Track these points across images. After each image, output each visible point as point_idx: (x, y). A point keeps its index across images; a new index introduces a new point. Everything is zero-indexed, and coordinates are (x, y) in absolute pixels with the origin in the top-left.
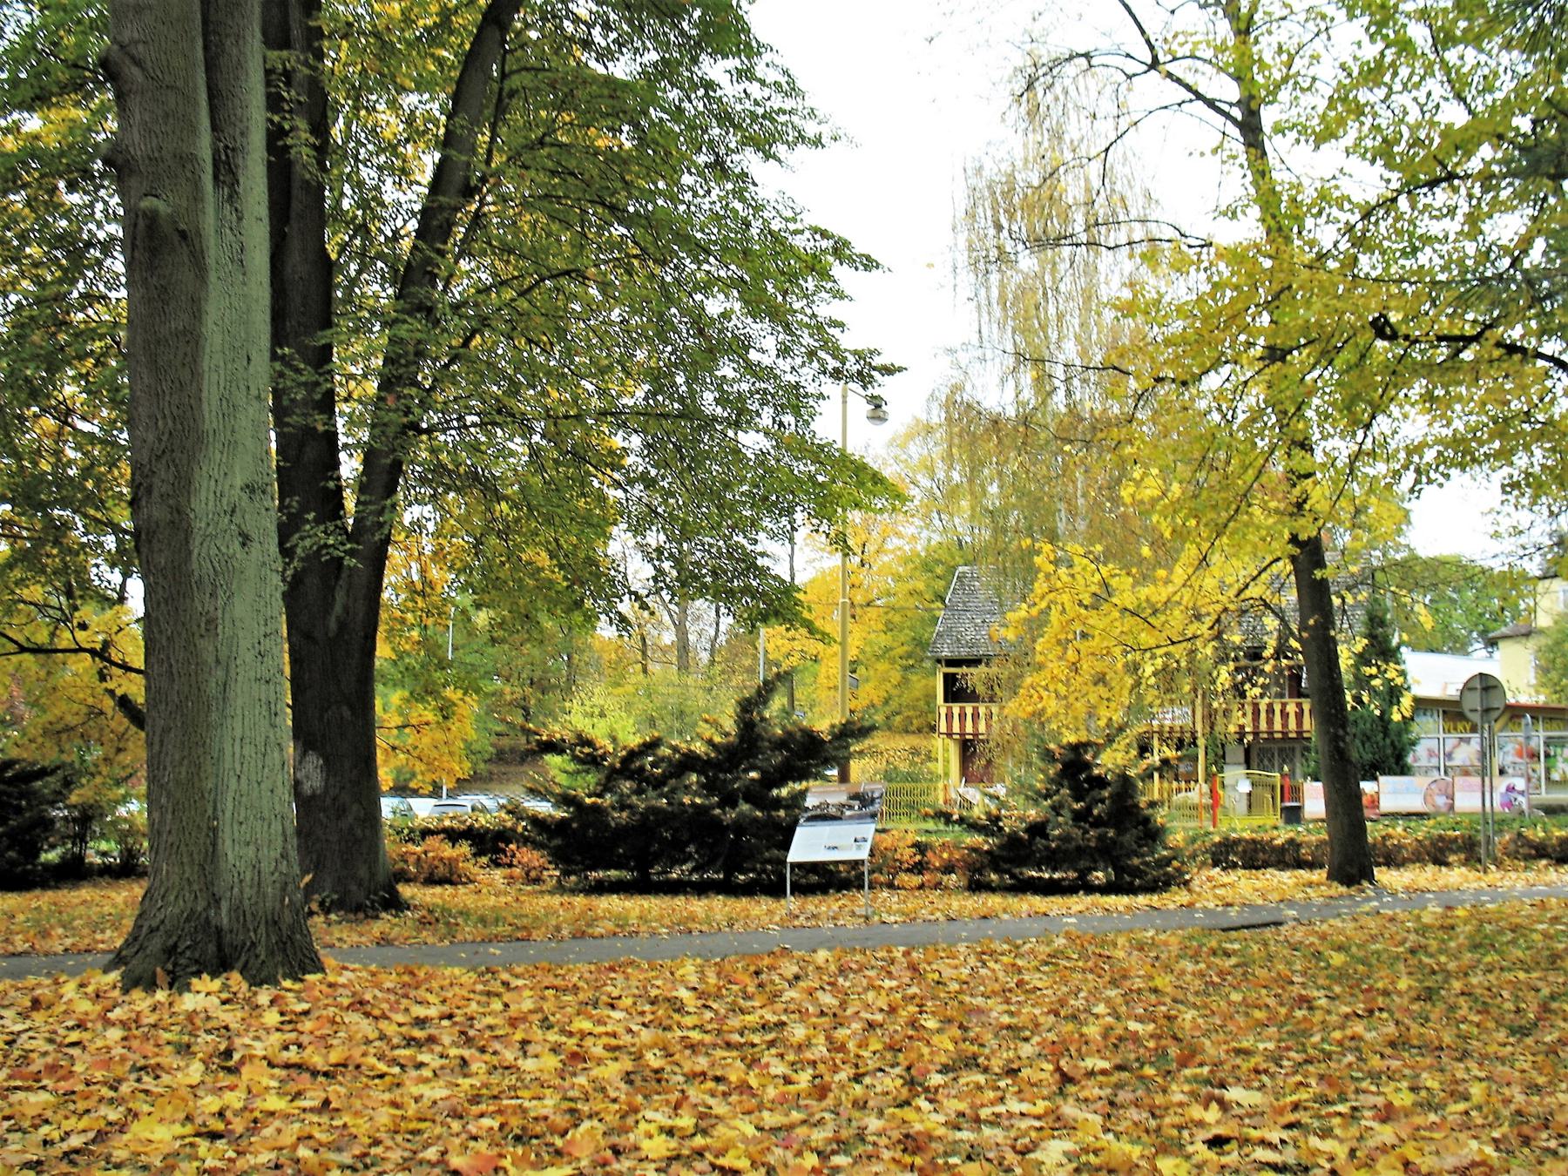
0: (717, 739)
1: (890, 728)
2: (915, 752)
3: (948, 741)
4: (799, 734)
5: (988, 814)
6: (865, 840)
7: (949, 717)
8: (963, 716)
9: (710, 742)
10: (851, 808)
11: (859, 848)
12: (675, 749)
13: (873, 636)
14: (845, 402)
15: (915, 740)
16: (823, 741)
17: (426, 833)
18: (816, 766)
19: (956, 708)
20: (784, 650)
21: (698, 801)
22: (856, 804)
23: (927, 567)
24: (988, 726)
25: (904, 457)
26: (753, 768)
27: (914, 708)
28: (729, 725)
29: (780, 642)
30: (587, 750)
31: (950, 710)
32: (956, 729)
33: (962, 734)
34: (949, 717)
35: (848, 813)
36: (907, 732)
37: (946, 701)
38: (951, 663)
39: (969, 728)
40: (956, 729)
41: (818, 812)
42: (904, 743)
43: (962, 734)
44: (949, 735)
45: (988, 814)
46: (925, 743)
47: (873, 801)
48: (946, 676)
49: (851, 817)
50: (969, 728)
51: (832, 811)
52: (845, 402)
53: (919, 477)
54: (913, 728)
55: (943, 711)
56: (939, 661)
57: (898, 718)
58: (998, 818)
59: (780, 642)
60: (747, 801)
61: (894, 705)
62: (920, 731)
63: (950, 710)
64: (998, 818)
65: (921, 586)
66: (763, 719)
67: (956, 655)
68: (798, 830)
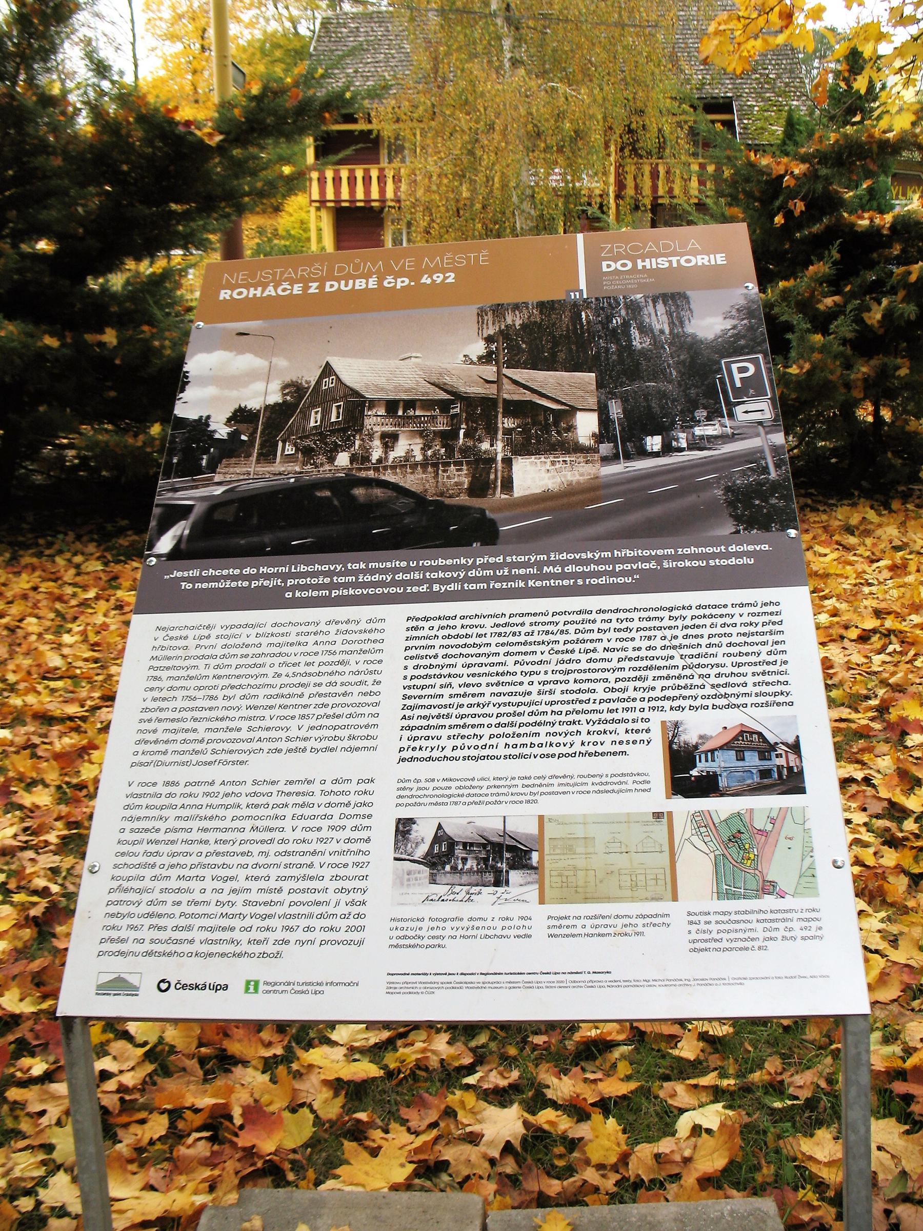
4: (138, 134)
7: (322, 181)
18: (186, 216)
32: (330, 195)
33: (337, 201)
34: (322, 181)
39: (345, 194)
40: (330, 195)
43: (337, 201)
46: (269, 222)
50: (345, 194)
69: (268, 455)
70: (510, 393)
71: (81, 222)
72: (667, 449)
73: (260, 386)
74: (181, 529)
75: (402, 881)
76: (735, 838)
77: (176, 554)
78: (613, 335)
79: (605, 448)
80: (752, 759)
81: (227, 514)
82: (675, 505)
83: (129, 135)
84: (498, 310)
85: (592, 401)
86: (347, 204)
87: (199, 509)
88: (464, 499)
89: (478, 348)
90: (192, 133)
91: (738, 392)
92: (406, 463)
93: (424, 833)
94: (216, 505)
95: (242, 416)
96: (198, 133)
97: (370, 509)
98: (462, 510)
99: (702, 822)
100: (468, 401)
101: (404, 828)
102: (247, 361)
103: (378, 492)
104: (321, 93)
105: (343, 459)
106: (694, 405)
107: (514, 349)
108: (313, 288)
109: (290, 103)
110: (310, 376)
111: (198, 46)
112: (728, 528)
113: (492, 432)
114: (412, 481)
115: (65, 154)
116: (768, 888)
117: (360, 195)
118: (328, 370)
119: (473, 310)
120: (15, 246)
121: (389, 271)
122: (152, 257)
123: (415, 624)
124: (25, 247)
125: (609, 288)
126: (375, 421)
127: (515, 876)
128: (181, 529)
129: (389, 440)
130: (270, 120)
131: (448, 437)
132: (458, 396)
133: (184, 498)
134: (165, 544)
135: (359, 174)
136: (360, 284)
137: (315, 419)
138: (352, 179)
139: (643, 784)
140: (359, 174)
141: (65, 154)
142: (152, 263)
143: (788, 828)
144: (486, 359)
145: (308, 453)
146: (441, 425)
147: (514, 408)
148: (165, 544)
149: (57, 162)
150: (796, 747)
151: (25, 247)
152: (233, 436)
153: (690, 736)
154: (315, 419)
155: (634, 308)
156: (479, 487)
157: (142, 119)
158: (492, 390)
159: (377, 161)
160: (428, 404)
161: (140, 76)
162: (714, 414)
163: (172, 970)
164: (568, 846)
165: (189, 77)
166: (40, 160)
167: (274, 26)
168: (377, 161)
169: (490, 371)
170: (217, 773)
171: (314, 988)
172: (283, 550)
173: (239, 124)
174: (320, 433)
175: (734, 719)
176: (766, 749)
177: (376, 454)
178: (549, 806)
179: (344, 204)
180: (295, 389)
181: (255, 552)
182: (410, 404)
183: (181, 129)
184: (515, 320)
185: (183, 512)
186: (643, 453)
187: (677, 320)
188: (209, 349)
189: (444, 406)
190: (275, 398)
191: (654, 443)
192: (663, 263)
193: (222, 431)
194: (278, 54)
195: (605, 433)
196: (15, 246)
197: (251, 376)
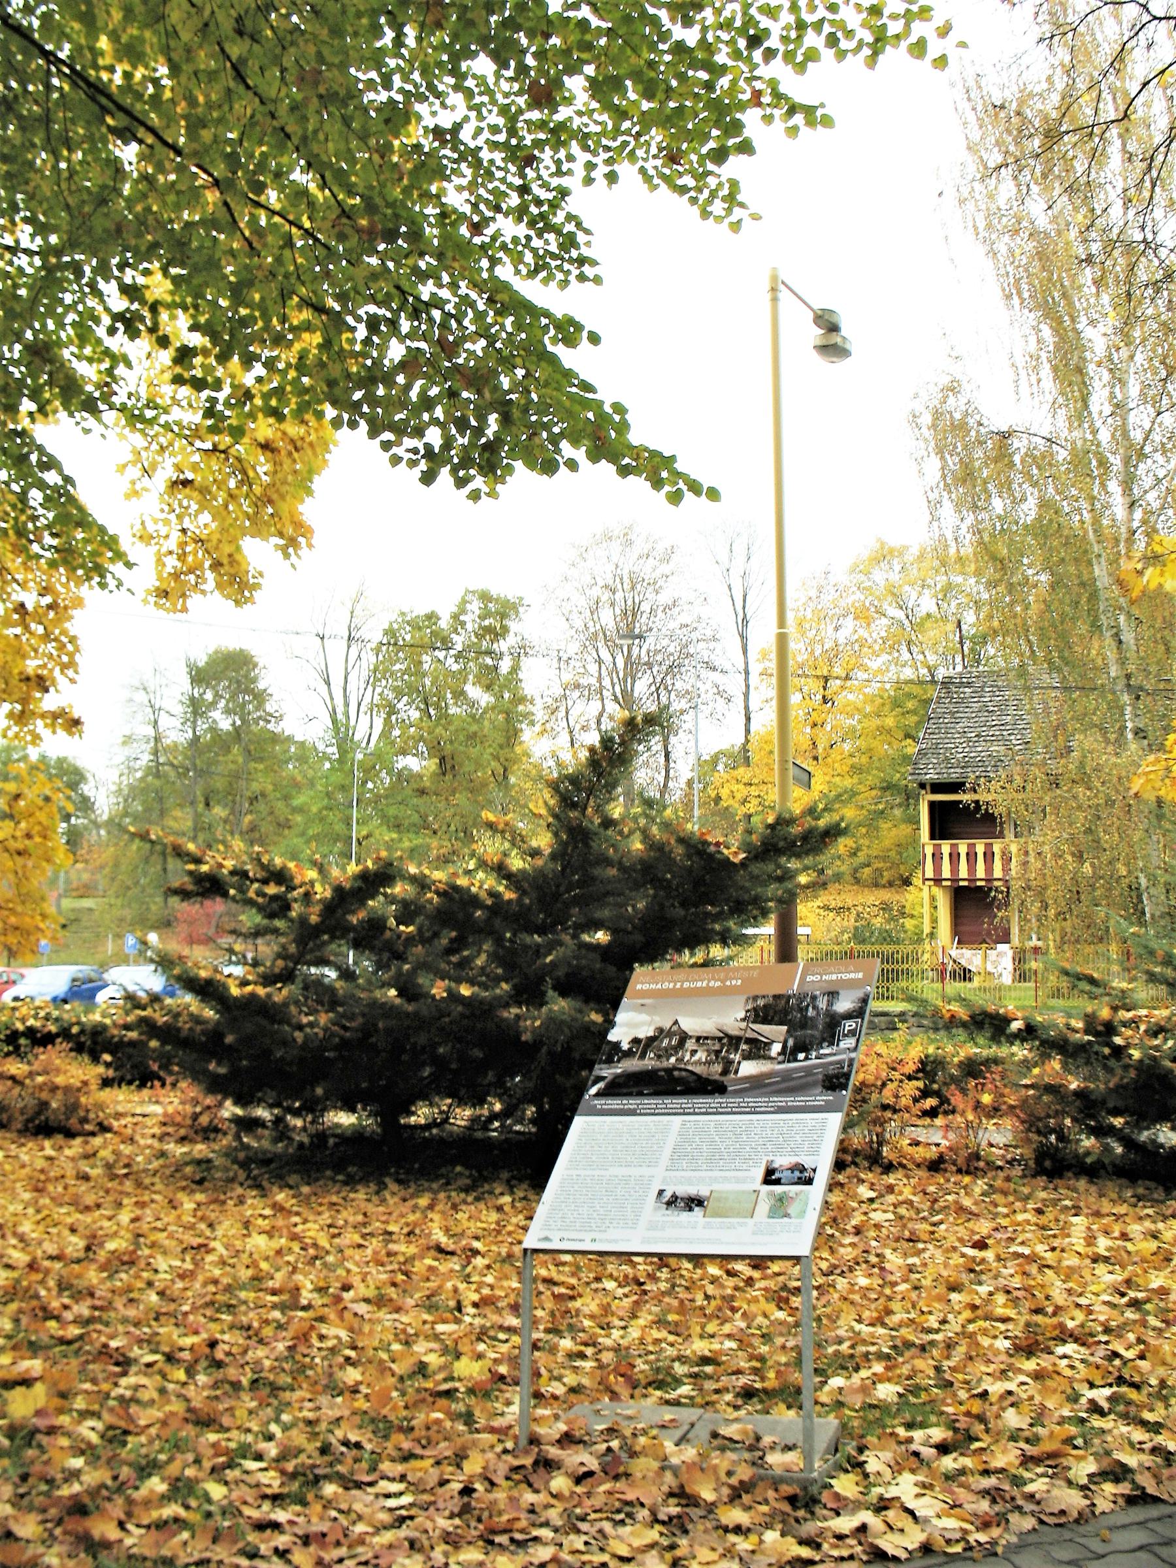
0: (516, 863)
1: (857, 881)
2: (885, 907)
3: (936, 891)
4: (679, 851)
5: (1090, 1020)
6: (805, 1178)
7: (937, 857)
8: (954, 857)
9: (501, 870)
10: (757, 1049)
11: (780, 1207)
12: (421, 883)
13: (837, 779)
14: (775, 300)
15: (886, 895)
16: (727, 862)
17: (41, 1039)
18: (718, 917)
19: (946, 847)
20: (739, 796)
21: (465, 991)
22: (775, 1033)
23: (896, 703)
24: (1006, 869)
25: (867, 584)
26: (597, 925)
27: (885, 859)
28: (543, 841)
29: (735, 787)
30: (272, 890)
31: (937, 847)
32: (946, 873)
33: (955, 880)
34: (937, 857)
35: (748, 1068)
36: (876, 885)
37: (932, 837)
38: (937, 788)
39: (963, 873)
40: (946, 873)
41: (649, 1062)
42: (873, 897)
43: (955, 880)
44: (938, 881)
45: (1090, 1020)
46: (897, 897)
47: (832, 1028)
48: (932, 805)
49: (756, 1084)
50: (963, 873)
51: (696, 1060)
52: (775, 300)
53: (885, 606)
54: (884, 881)
55: (929, 850)
56: (922, 786)
57: (867, 870)
58: (1110, 1029)
59: (735, 787)
60: (564, 990)
61: (862, 857)
62: (891, 884)
63: (937, 847)
64: (1110, 1029)
65: (890, 722)
66: (608, 823)
67: (944, 778)
68: (579, 1122)
69: (643, 1056)
70: (750, 1034)
71: (630, 920)
72: (806, 1058)
73: (645, 1028)
74: (601, 1085)
75: (656, 1209)
76: (781, 1200)
77: (598, 1095)
78: (801, 1010)
79: (781, 1058)
80: (797, 1174)
81: (621, 1080)
82: (804, 1081)
83: (671, 852)
84: (755, 998)
85: (782, 1039)
86: (965, 883)
87: (610, 1078)
88: (717, 1077)
89: (742, 1014)
90: (720, 852)
91: (845, 1035)
92: (699, 1062)
93: (667, 1195)
94: (617, 1076)
95: (636, 1041)
96: (725, 851)
97: (679, 1081)
98: (715, 1081)
99: (772, 1194)
100: (730, 1037)
101: (661, 1192)
102: (644, 1017)
103: (684, 1074)
104: (822, 823)
105: (673, 1060)
106: (824, 1040)
107: (757, 1015)
108: (678, 985)
109: (795, 830)
110: (667, 1025)
111: (819, 697)
112: (820, 1089)
113: (736, 1050)
114: (698, 1069)
115: (622, 868)
116: (787, 1215)
117: (981, 873)
118: (676, 1022)
119: (743, 998)
120: (575, 936)
121: (713, 979)
122: (692, 949)
123: (684, 1124)
124: (586, 938)
125: (808, 989)
126: (690, 1045)
127: (697, 1209)
128: (601, 1085)
129: (694, 1052)
130: (781, 844)
131: (718, 1052)
132: (727, 1035)
133: (604, 1073)
134: (593, 1090)
135: (980, 849)
136: (699, 984)
137: (665, 1043)
138: (972, 857)
139: (753, 1179)
140: (980, 849)
141: (622, 868)
142: (692, 955)
143: (802, 1197)
144: (743, 1020)
145: (659, 1057)
146: (717, 1047)
147: (749, 1041)
148: (593, 1090)
149: (612, 872)
150: (814, 1170)
151: (586, 938)
152: (630, 1049)
153: (776, 1165)
154: (665, 1043)
155: (814, 998)
156: (725, 1072)
157: (681, 841)
158: (741, 1033)
159: (1001, 835)
160: (713, 1038)
161: (752, 729)
162: (831, 1044)
163: (566, 1235)
164: (718, 1200)
165: (808, 730)
166: (597, 871)
167: (908, 673)
168: (1001, 835)
169: (743, 1025)
170: (597, 1173)
171: (616, 1241)
172: (640, 1094)
173: (756, 847)
174: (666, 1049)
175: (794, 1160)
176: (803, 1169)
177: (687, 1058)
178: (716, 1187)
179: (962, 883)
180: (660, 1030)
181: (629, 1095)
182: (706, 1038)
183: (712, 849)
184: (761, 1002)
185: (603, 1078)
186: (796, 1060)
187: (830, 1004)
188: (628, 1010)
189: (720, 1039)
190: (651, 1034)
191: (801, 1056)
192: (834, 977)
193: (625, 1046)
194: (910, 705)
195: (783, 1052)
196: (575, 936)
197: (643, 1024)
